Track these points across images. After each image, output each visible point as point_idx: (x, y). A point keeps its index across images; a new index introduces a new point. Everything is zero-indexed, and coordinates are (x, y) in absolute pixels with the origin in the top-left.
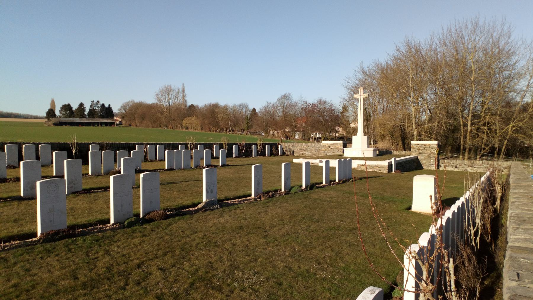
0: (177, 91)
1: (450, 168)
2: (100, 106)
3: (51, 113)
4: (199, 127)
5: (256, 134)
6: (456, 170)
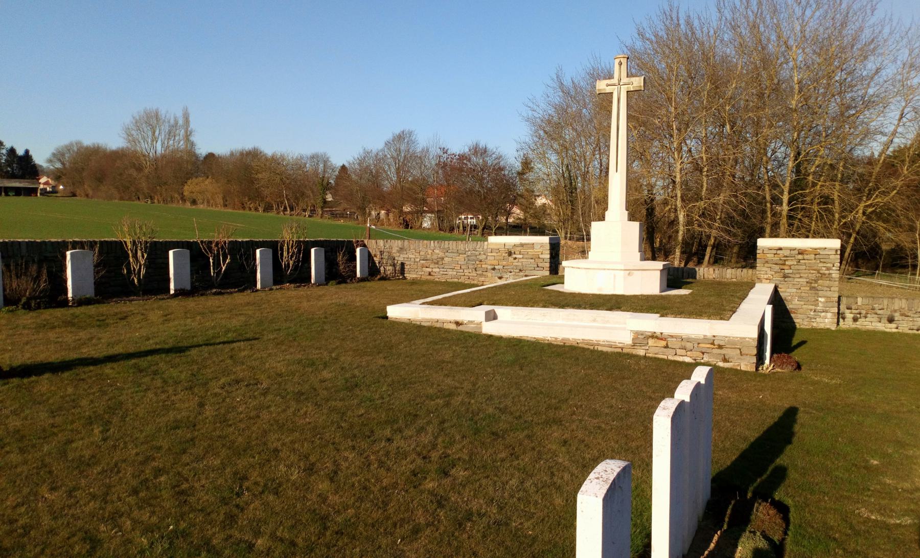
0: (172, 122)
1: (871, 324)
4: (220, 200)
5: (342, 216)
6: (891, 328)
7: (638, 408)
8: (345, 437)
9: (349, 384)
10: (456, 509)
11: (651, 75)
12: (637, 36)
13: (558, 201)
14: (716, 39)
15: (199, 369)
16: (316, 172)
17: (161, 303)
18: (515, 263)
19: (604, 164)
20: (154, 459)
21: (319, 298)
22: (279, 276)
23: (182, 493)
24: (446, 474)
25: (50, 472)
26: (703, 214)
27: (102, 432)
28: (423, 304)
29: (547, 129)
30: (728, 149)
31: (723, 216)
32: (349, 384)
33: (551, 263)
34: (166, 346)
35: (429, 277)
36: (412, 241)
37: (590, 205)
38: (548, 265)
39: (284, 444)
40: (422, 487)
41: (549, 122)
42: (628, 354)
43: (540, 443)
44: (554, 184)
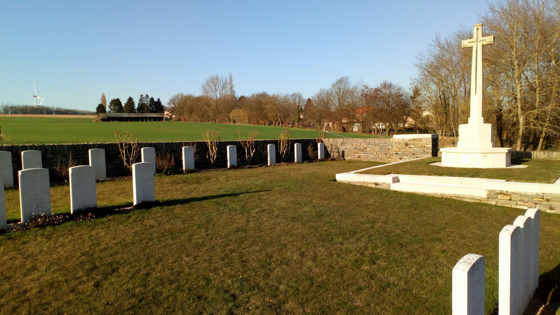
0: (224, 81)
2: (149, 100)
3: (101, 108)
4: (247, 120)
5: (309, 126)
7: (491, 235)
8: (319, 240)
9: (318, 214)
10: (381, 281)
11: (499, 33)
12: (489, 10)
13: (437, 113)
14: (544, 7)
15: (245, 204)
16: (295, 104)
17: (224, 172)
18: (410, 150)
19: (467, 89)
20: (229, 245)
21: (299, 170)
22: (279, 159)
23: (243, 261)
24: (374, 263)
25: (186, 249)
26: (537, 117)
27: (205, 232)
28: (356, 173)
29: (430, 70)
30: (554, 76)
31: (551, 118)
32: (318, 214)
33: (433, 150)
34: (229, 193)
35: (358, 159)
36: (349, 139)
37: (458, 115)
38: (431, 151)
39: (288, 242)
40: (361, 268)
41: (431, 66)
42: (484, 204)
43: (428, 251)
44: (434, 103)
